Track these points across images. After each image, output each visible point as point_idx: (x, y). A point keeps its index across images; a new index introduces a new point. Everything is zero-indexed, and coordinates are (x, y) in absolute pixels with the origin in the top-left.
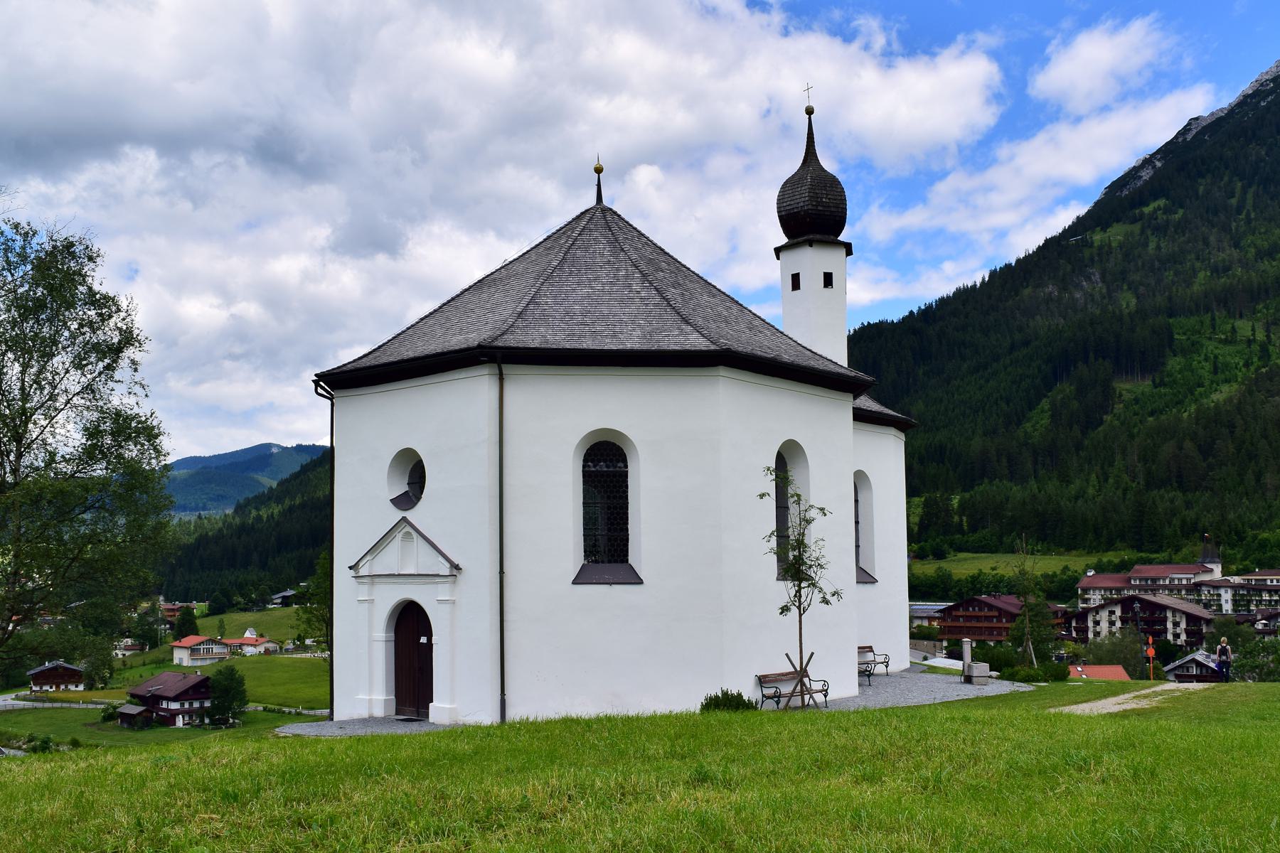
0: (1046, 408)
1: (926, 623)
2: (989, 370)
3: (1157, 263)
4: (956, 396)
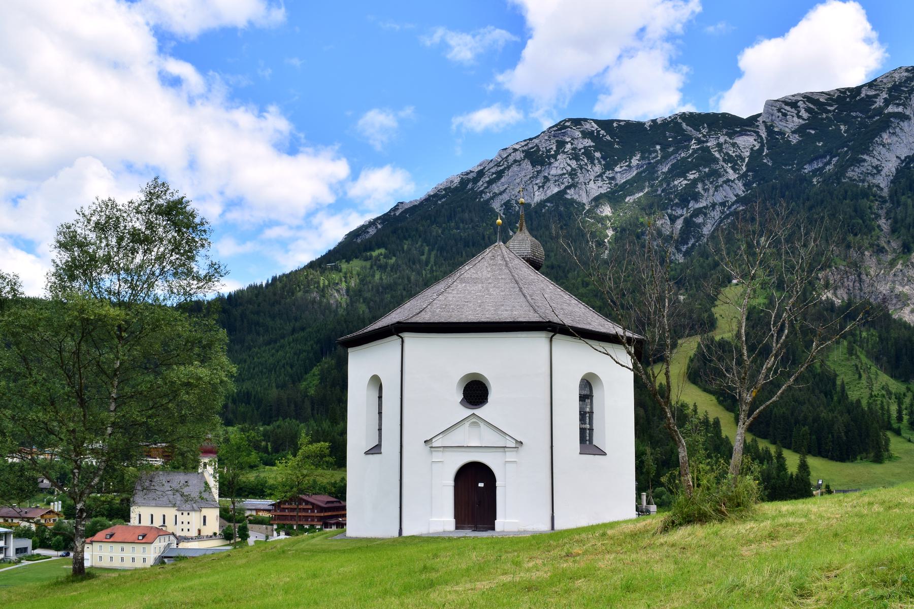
0: (317, 373)
1: (254, 513)
2: (278, 344)
3: (380, 288)
4: (256, 359)
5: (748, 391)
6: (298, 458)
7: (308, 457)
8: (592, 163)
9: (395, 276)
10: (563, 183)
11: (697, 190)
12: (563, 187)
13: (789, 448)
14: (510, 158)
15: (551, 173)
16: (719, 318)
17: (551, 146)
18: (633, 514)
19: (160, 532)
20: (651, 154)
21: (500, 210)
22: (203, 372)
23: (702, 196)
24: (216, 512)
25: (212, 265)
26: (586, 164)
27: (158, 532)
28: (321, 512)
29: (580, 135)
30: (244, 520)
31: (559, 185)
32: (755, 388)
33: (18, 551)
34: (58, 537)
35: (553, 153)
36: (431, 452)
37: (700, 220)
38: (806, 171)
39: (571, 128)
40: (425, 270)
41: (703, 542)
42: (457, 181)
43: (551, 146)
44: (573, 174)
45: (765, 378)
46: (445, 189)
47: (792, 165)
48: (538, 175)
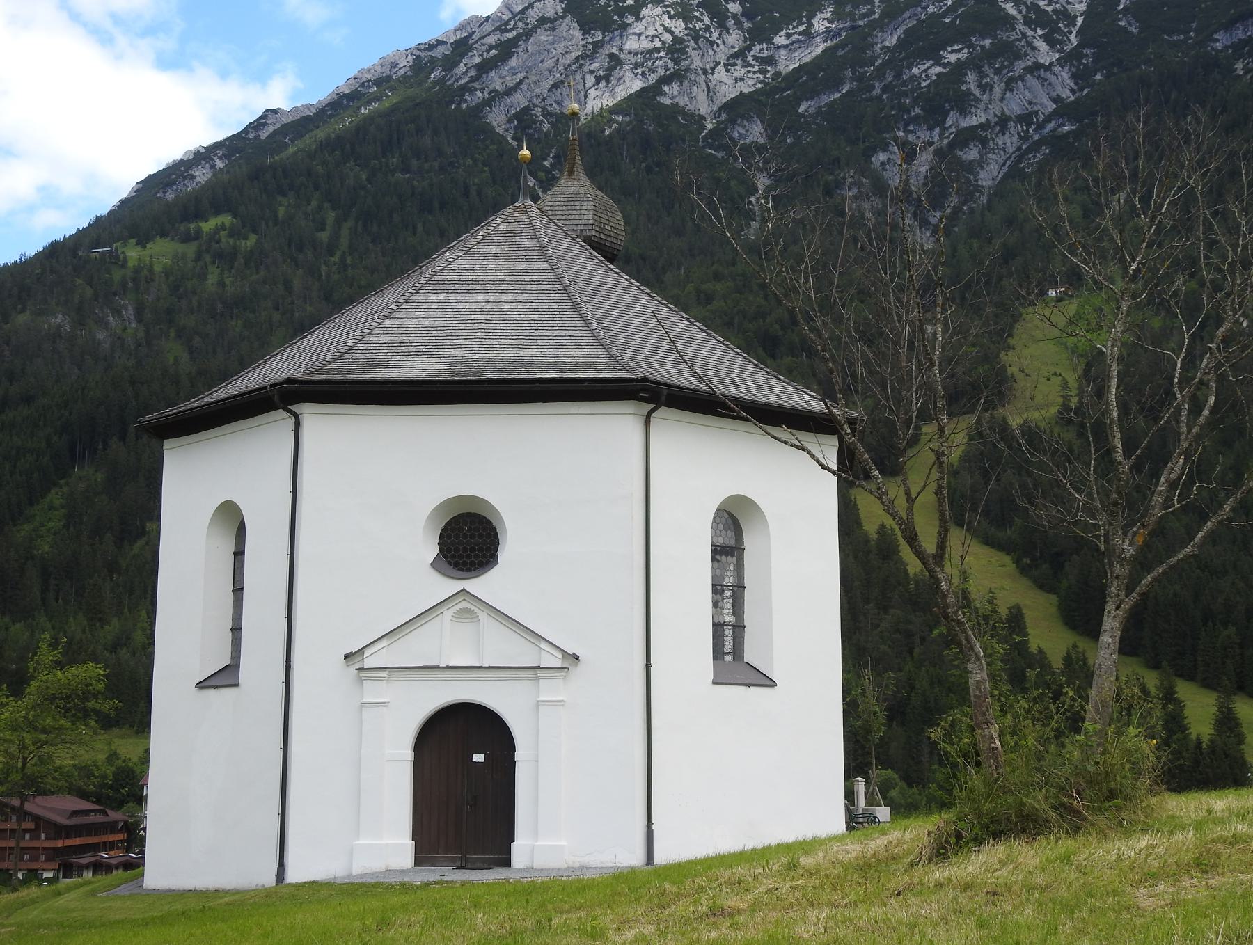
0: (57, 503)
3: (220, 306)
5: (1125, 534)
6: (27, 701)
7: (52, 699)
8: (723, 26)
9: (255, 277)
10: (653, 71)
11: (964, 88)
12: (653, 78)
13: (1190, 678)
14: (531, 12)
16: (1019, 376)
18: (838, 824)
20: (858, 7)
23: (978, 100)
26: (708, 29)
28: (57, 837)
32: (1143, 525)
36: (361, 681)
37: (972, 154)
38: (1219, 46)
40: (326, 263)
41: (1040, 879)
42: (405, 63)
44: (676, 49)
45: (1165, 501)
46: (378, 82)
47: (1186, 32)
48: (595, 52)
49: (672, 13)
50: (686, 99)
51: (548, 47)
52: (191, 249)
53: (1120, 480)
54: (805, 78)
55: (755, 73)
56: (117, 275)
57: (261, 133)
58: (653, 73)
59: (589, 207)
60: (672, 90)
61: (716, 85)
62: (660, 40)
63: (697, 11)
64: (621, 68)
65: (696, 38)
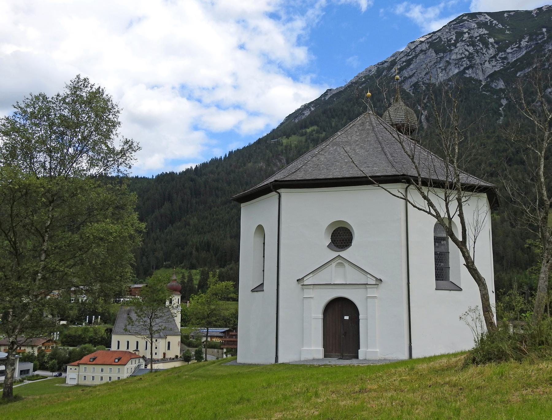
4: (215, 216)
7: (216, 294)
10: (462, 65)
12: (462, 68)
14: (417, 48)
15: (452, 58)
17: (452, 37)
19: (132, 356)
20: (538, 36)
21: (410, 91)
22: (114, 228)
24: (178, 339)
25: (126, 142)
26: (482, 49)
27: (130, 356)
29: (476, 26)
30: (200, 345)
31: (458, 67)
33: (22, 372)
34: (54, 361)
35: (453, 42)
36: (303, 289)
39: (468, 21)
42: (374, 70)
43: (452, 37)
44: (470, 57)
46: (365, 77)
48: (441, 60)
49: (468, 44)
50: (475, 74)
51: (424, 60)
52: (303, 139)
53: (546, 208)
54: (519, 64)
55: (500, 63)
56: (280, 148)
57: (326, 97)
58: (462, 66)
59: (403, 113)
60: (469, 72)
61: (485, 69)
62: (464, 54)
63: (478, 43)
64: (450, 65)
65: (477, 53)
